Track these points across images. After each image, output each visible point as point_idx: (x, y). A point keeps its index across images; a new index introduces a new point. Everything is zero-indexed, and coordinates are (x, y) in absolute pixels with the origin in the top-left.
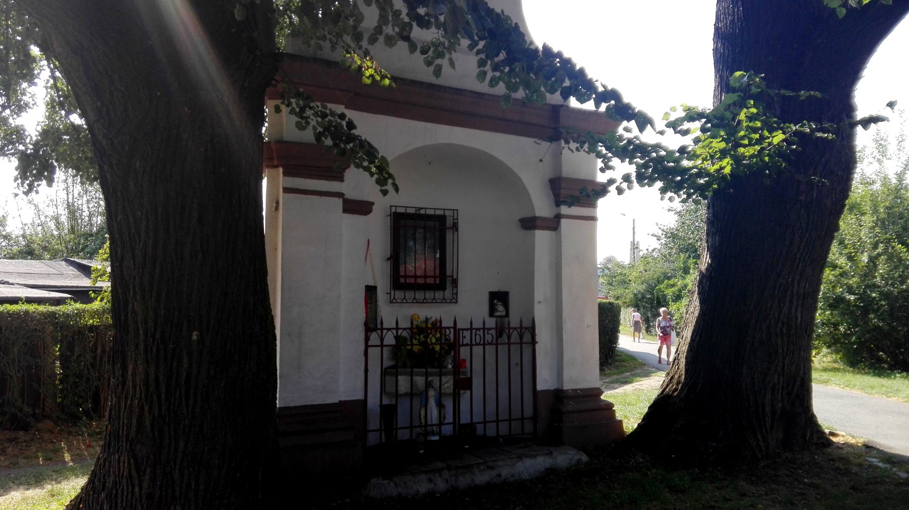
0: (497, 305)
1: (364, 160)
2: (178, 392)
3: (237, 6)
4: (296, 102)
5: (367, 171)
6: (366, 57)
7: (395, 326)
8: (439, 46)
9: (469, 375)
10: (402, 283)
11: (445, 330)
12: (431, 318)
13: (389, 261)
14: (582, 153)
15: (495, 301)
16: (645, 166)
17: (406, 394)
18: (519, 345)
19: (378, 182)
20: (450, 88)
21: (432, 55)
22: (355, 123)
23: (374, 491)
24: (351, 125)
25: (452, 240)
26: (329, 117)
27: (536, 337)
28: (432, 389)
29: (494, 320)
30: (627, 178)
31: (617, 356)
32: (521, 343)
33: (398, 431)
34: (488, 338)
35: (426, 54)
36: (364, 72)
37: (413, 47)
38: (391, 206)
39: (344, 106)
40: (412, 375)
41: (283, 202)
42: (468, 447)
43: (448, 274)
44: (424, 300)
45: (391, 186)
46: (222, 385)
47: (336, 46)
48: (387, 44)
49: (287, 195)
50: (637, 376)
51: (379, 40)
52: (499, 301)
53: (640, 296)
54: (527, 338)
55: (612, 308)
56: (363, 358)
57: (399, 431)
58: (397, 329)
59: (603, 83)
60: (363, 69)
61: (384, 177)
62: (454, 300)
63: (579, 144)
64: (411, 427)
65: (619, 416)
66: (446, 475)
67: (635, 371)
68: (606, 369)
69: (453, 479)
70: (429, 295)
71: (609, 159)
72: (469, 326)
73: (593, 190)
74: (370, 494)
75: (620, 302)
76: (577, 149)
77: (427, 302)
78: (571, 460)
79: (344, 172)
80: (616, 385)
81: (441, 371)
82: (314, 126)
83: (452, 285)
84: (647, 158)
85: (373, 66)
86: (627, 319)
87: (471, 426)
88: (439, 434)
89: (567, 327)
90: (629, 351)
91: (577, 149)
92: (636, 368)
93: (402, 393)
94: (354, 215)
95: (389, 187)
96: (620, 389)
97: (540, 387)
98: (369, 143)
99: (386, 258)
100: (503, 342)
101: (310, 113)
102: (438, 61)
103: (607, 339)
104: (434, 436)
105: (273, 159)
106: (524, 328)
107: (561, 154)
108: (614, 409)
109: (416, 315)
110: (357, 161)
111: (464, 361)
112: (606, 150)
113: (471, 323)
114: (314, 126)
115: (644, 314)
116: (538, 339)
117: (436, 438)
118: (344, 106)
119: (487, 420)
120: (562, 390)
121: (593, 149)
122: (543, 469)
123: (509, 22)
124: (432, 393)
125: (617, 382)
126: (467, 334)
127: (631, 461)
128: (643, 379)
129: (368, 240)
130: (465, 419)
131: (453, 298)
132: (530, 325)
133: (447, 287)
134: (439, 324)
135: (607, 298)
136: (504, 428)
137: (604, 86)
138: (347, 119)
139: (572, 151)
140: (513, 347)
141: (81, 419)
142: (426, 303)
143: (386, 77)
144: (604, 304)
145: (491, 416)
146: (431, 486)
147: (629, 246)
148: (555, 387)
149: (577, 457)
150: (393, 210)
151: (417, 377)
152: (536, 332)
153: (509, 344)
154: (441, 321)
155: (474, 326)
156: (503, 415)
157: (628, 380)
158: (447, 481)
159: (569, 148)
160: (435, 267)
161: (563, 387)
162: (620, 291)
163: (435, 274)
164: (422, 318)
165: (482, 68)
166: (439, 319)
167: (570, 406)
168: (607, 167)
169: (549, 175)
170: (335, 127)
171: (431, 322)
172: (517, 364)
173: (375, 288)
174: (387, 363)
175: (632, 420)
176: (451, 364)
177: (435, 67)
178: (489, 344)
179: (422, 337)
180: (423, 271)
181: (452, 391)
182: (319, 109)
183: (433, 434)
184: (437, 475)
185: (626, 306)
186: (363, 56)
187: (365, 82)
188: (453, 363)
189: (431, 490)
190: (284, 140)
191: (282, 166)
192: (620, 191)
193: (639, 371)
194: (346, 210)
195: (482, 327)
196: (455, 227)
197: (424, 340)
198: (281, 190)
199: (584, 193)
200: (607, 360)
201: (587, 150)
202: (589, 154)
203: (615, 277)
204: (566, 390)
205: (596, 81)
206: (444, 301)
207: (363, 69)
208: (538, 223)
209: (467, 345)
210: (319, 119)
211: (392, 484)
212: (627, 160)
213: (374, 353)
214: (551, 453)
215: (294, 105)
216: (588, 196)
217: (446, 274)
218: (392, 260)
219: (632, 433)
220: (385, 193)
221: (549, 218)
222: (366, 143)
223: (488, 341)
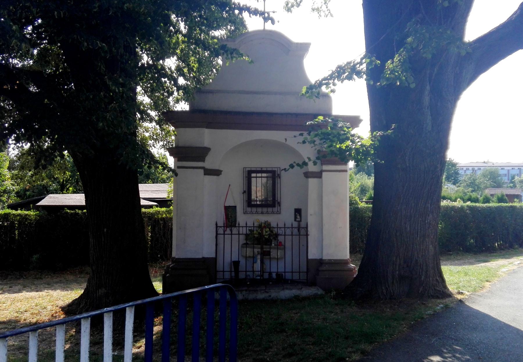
15: (297, 213)
38: (244, 168)
40: (254, 248)
54: (303, 232)
56: (215, 240)
62: (279, 213)
66: (244, 293)
77: (247, 214)
81: (270, 247)
89: (325, 227)
97: (310, 257)
113: (285, 225)
116: (309, 233)
119: (293, 271)
131: (278, 211)
132: (305, 226)
141: (159, 260)
184: (240, 292)
194: (205, 174)
206: (273, 213)
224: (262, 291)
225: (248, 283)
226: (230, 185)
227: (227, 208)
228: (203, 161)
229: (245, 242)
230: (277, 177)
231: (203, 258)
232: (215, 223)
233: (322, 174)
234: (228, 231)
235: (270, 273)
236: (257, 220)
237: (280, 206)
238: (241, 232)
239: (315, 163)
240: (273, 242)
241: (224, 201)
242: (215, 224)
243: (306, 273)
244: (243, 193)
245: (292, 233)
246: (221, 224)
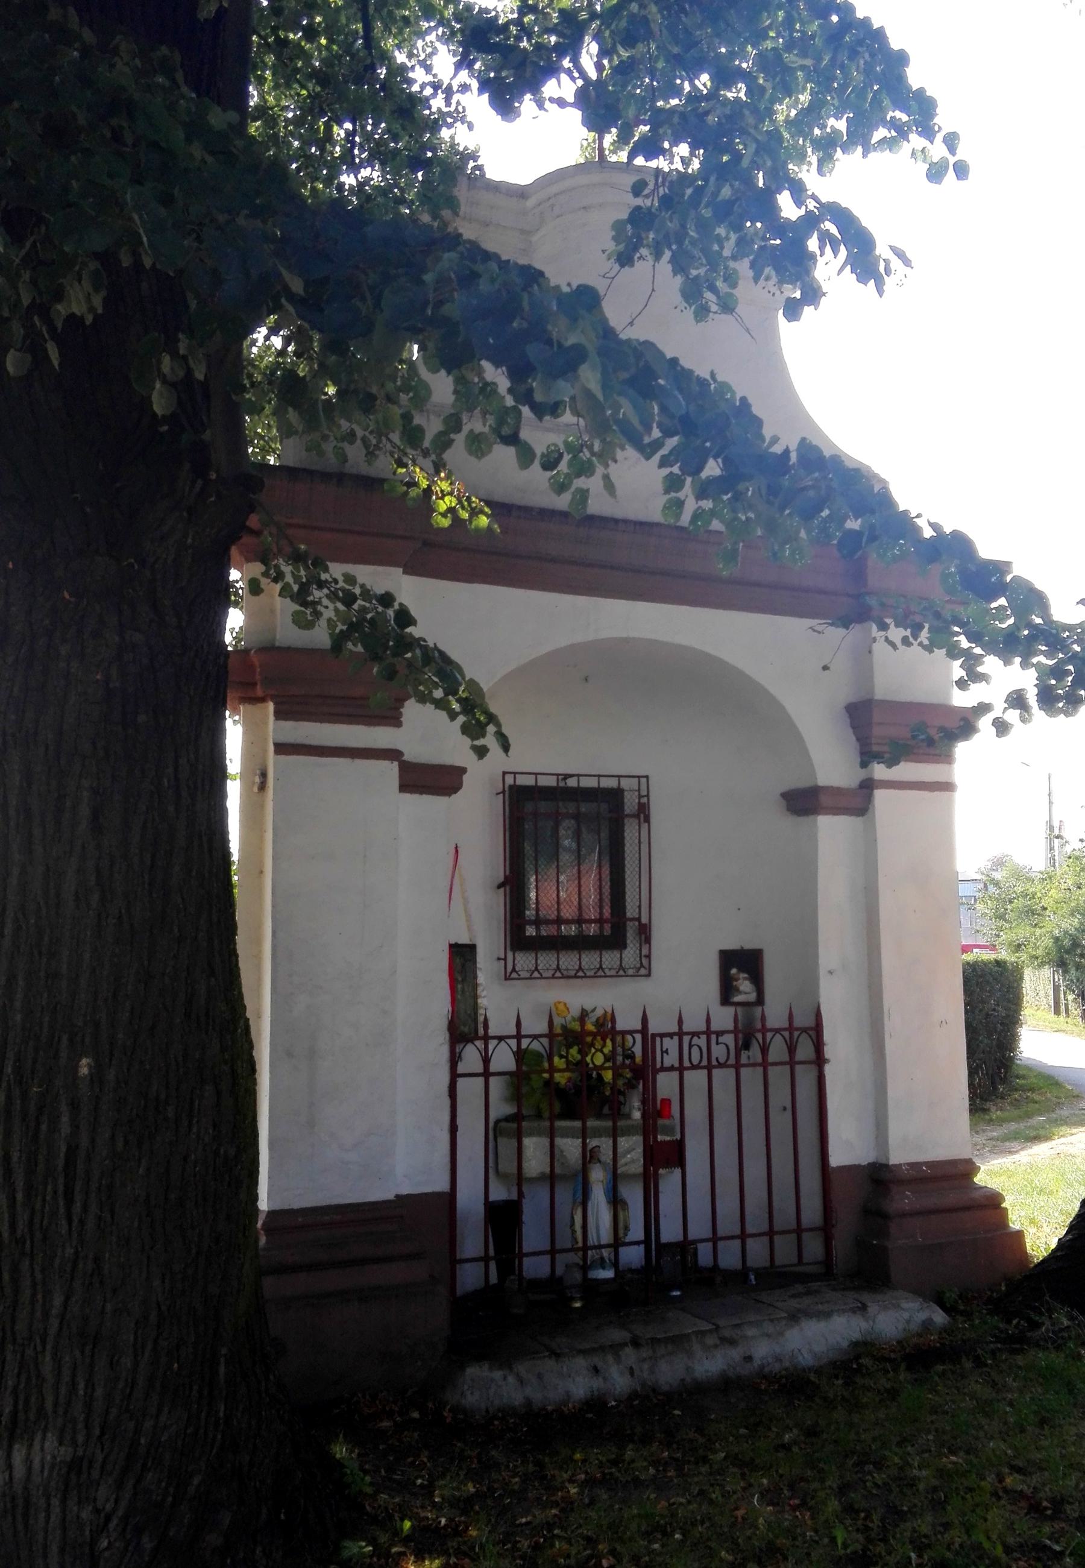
0: (737, 980)
1: (436, 686)
2: (49, 1188)
3: (158, 385)
4: (292, 573)
5: (443, 709)
6: (437, 473)
7: (514, 1032)
8: (581, 451)
9: (678, 1137)
10: (531, 937)
11: (623, 1039)
12: (595, 1008)
13: (502, 889)
14: (916, 648)
15: (734, 971)
16: (1058, 672)
17: (541, 1178)
18: (788, 1067)
19: (465, 730)
20: (626, 521)
21: (566, 470)
22: (414, 612)
24: (405, 618)
25: (637, 841)
26: (360, 602)
27: (825, 1048)
28: (598, 1164)
29: (730, 1011)
30: (1017, 700)
31: (1018, 1077)
32: (792, 1063)
33: (525, 1259)
34: (719, 1052)
35: (552, 470)
36: (435, 503)
37: (526, 455)
38: (504, 773)
39: (401, 569)
41: (274, 773)
42: (678, 1293)
43: (629, 915)
44: (578, 971)
45: (494, 739)
46: (141, 1171)
47: (377, 452)
48: (470, 452)
49: (283, 758)
50: (1062, 1125)
51: (455, 443)
52: (741, 970)
53: (1067, 943)
54: (804, 1051)
55: (1002, 974)
56: (447, 1102)
57: (525, 1260)
58: (519, 1037)
59: (932, 521)
60: (434, 497)
61: (478, 721)
62: (644, 969)
63: (909, 630)
64: (553, 1252)
65: (1015, 1221)
66: (630, 1355)
67: (1058, 1111)
68: (993, 1108)
69: (646, 1366)
70: (590, 959)
71: (978, 659)
72: (676, 1029)
73: (942, 729)
74: (463, 1401)
75: (1024, 957)
76: (906, 641)
77: (586, 977)
78: (908, 1322)
79: (402, 707)
80: (1015, 1145)
82: (329, 620)
83: (637, 938)
84: (1061, 655)
85: (453, 490)
86: (1042, 994)
87: (685, 1247)
88: (615, 1264)
90: (1045, 1066)
91: (906, 641)
92: (1059, 1105)
93: (534, 1175)
94: (424, 796)
95: (489, 740)
96: (1023, 1153)
97: (837, 1158)
98: (442, 654)
99: (496, 884)
100: (752, 1061)
101: (322, 595)
102: (580, 483)
103: (994, 1043)
104: (604, 1268)
105: (255, 684)
106: (797, 1029)
107: (870, 652)
108: (1003, 1205)
109: (562, 1004)
110: (421, 688)
111: (666, 1102)
112: (970, 641)
113: (680, 1022)
114: (329, 620)
115: (1078, 980)
116: (828, 1052)
117: (608, 1274)
118: (401, 569)
120: (886, 1166)
121: (941, 640)
122: (845, 1344)
123: (729, 396)
124: (598, 1176)
125: (1016, 1139)
126: (671, 1044)
127: (1043, 1324)
128: (1074, 1131)
129: (456, 848)
130: (670, 1232)
131: (642, 965)
132: (810, 1022)
133: (628, 942)
134: (610, 1025)
135: (993, 948)
136: (758, 1252)
137: (934, 526)
138: (396, 606)
139: (893, 645)
140: (772, 1071)
142: (582, 977)
143: (482, 512)
144: (985, 964)
145: (728, 1224)
146: (597, 1383)
147: (1042, 832)
148: (871, 1160)
149: (922, 1316)
150: (509, 780)
151: (565, 1140)
152: (825, 1038)
153: (765, 1064)
154: (613, 1020)
155: (685, 1029)
156: (756, 1222)
157: (1042, 1132)
158: (632, 1373)
159: (887, 639)
160: (601, 900)
161: (888, 1159)
162: (1022, 932)
163: (601, 913)
164: (575, 1012)
165: (673, 494)
166: (609, 1011)
167: (904, 1200)
168: (973, 675)
169: (845, 694)
170: (372, 621)
171: (594, 1019)
172: (785, 1109)
173: (472, 948)
174: (500, 1108)
175: (1047, 1230)
176: (639, 1109)
177: (574, 495)
178: (720, 1065)
179: (574, 1051)
180: (576, 910)
181: (641, 1170)
182: (338, 586)
183: (602, 1264)
184: (610, 1358)
185: (1038, 965)
186: (432, 471)
187: (437, 523)
188: (641, 1107)
189: (596, 1393)
190: (277, 644)
191: (273, 698)
192: (1001, 727)
193: (1065, 1112)
194: (406, 786)
195: (705, 1029)
196: (643, 812)
197: (579, 1057)
198: (271, 748)
199: (922, 737)
200: (995, 1089)
201: (926, 642)
202: (931, 651)
203: (1011, 902)
204: (895, 1165)
205: (919, 516)
206: (621, 972)
207: (434, 497)
208: (824, 800)
209: (672, 1068)
210: (341, 606)
211: (511, 1379)
212: (1018, 660)
213: (470, 1089)
214: (864, 1308)
215: (289, 579)
216: (931, 742)
217: (625, 913)
218: (508, 888)
219: (1045, 1261)
220: (481, 752)
221: (848, 789)
222: (437, 654)
223: (717, 1059)
225: (578, 1305)
229: (509, 1109)
233: (869, 799)
242: (705, 1021)
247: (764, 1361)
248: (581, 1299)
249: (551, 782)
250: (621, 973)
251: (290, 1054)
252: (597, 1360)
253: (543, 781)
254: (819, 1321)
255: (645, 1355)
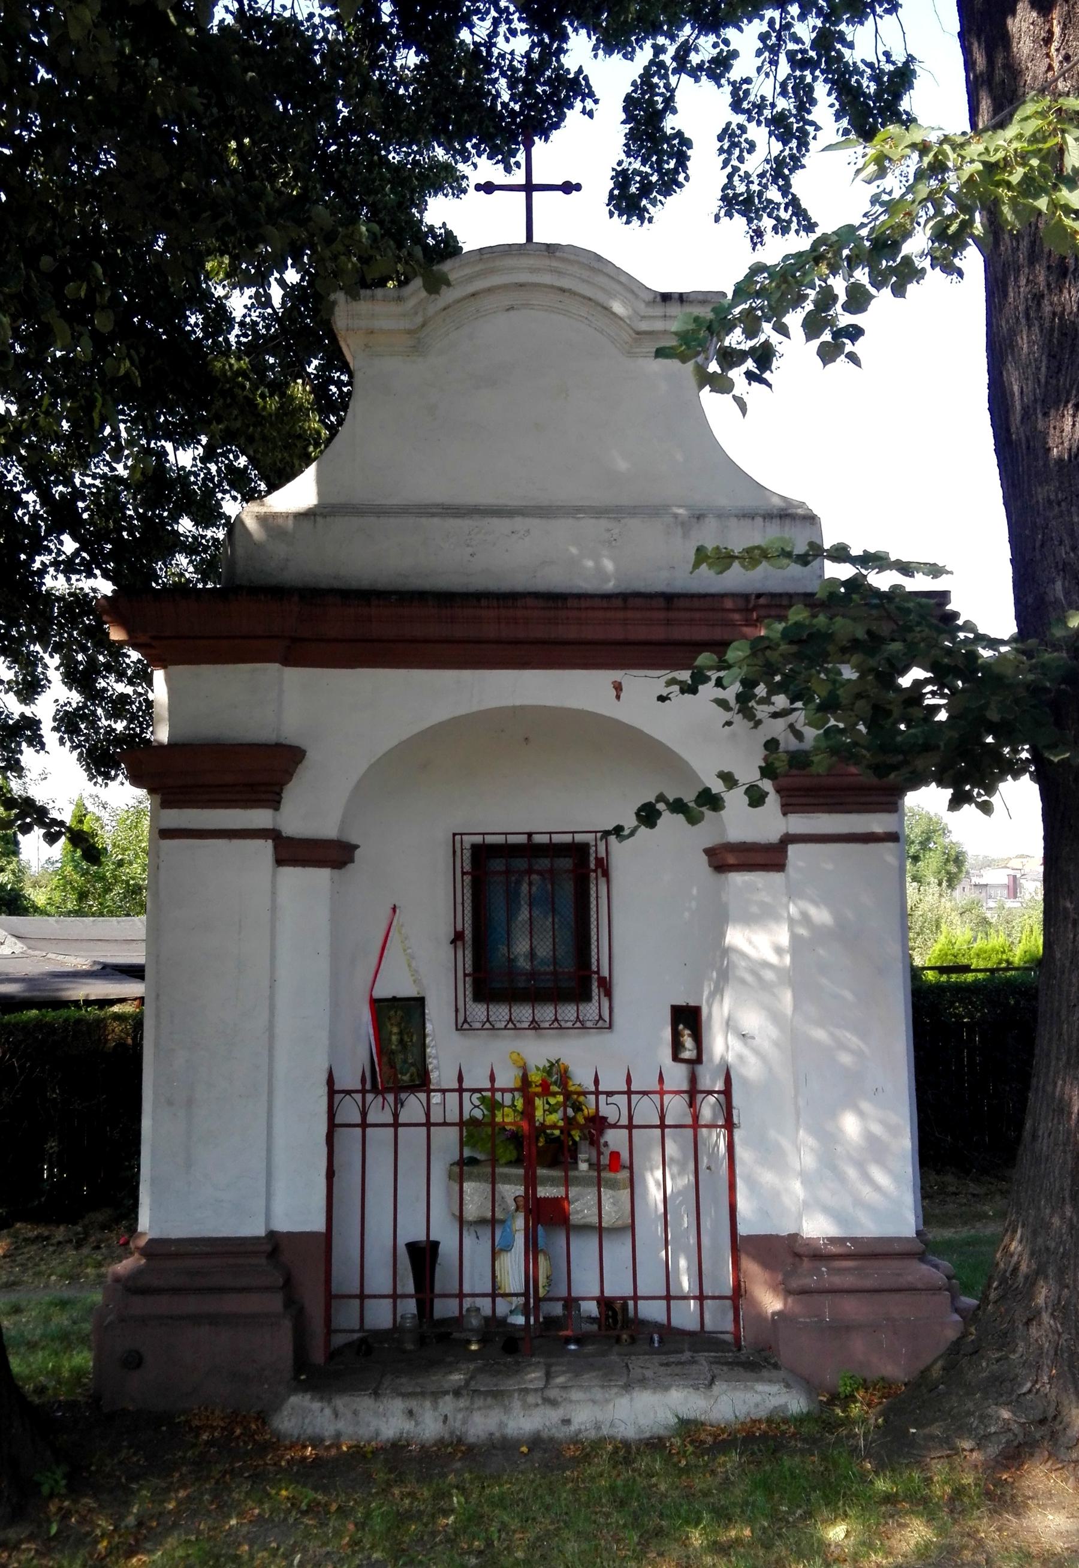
17: (481, 1222)
23: (289, 1420)
38: (454, 835)
52: (687, 1027)
69: (460, 1416)
78: (757, 1405)
81: (566, 1176)
131: (601, 1017)
146: (408, 1426)
151: (507, 1187)
184: (428, 1404)
194: (280, 861)
206: (581, 1025)
211: (328, 1411)
224: (531, 1399)
226: (394, 909)
227: (382, 1009)
228: (274, 801)
230: (595, 871)
231: (272, 1235)
232: (324, 1077)
234: (379, 1113)
235: (571, 1302)
236: (514, 1056)
237: (609, 993)
238: (436, 1117)
239: (756, 798)
240: (582, 1156)
241: (370, 984)
243: (728, 1303)
244: (453, 942)
245: (662, 1117)
246: (349, 1078)
247: (583, 1427)
248: (478, 1342)
249: (523, 839)
250: (578, 1025)
251: (170, 1103)
252: (413, 1404)
253: (513, 839)
254: (655, 1393)
255: (462, 1405)
